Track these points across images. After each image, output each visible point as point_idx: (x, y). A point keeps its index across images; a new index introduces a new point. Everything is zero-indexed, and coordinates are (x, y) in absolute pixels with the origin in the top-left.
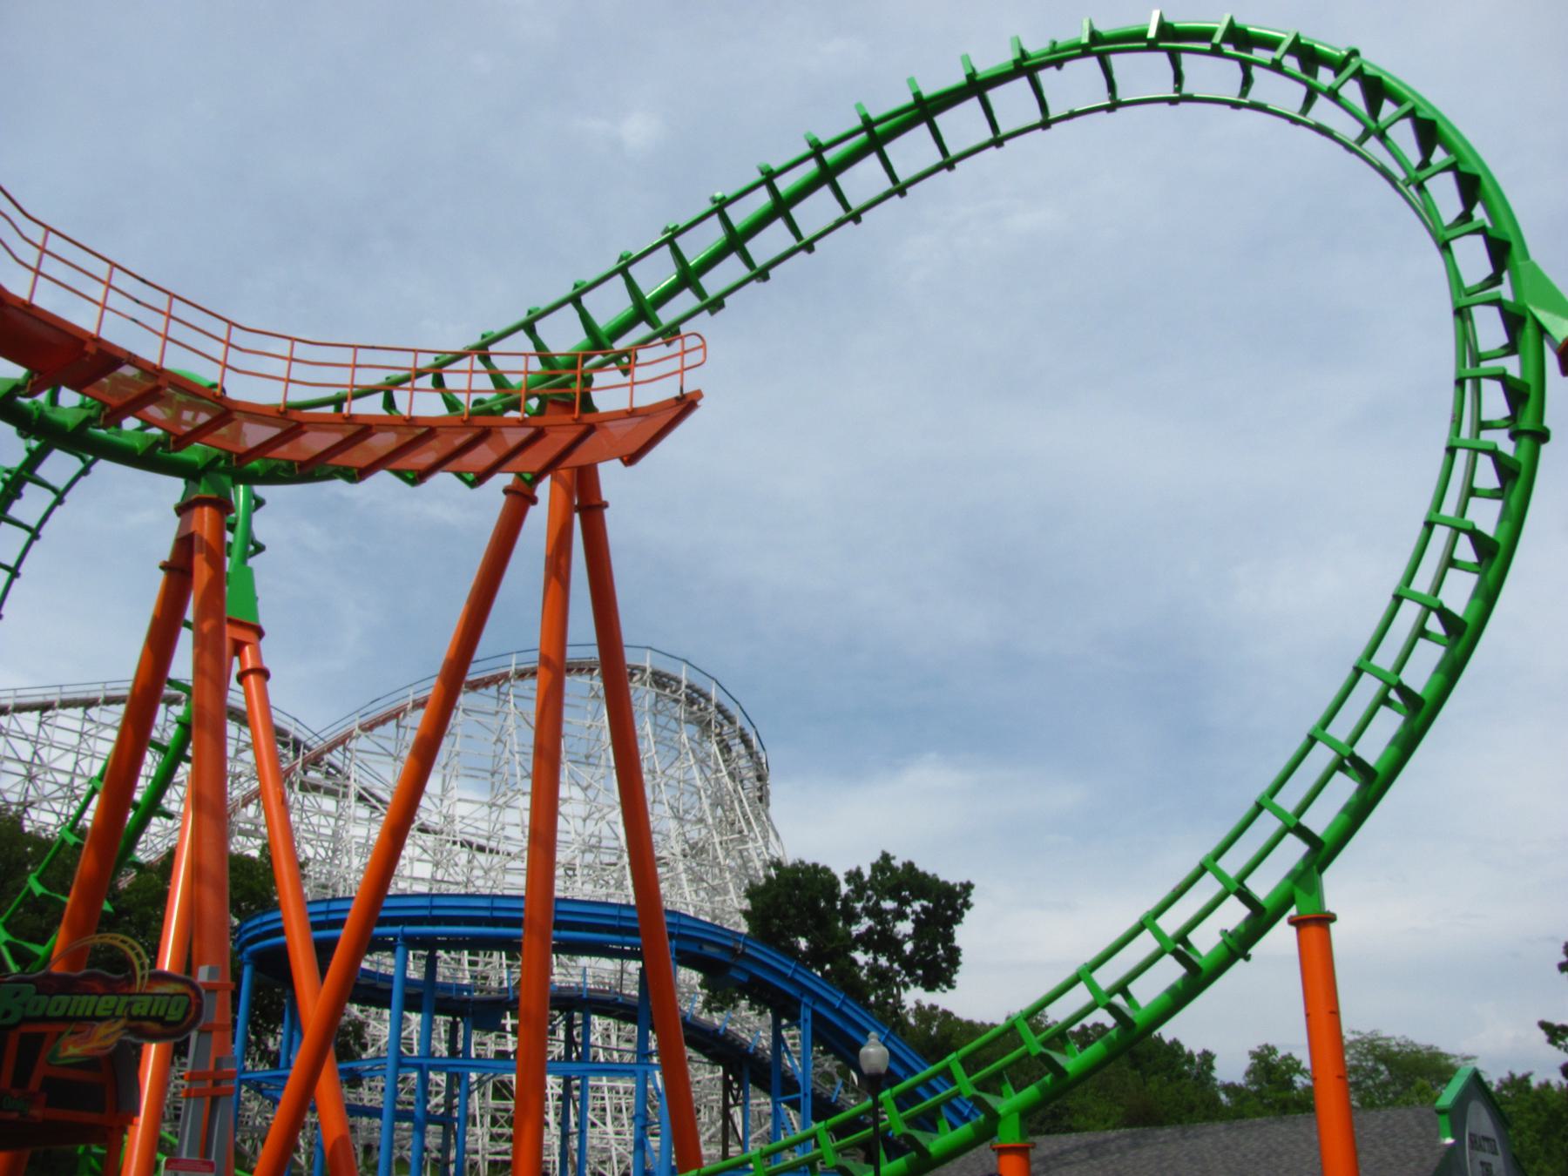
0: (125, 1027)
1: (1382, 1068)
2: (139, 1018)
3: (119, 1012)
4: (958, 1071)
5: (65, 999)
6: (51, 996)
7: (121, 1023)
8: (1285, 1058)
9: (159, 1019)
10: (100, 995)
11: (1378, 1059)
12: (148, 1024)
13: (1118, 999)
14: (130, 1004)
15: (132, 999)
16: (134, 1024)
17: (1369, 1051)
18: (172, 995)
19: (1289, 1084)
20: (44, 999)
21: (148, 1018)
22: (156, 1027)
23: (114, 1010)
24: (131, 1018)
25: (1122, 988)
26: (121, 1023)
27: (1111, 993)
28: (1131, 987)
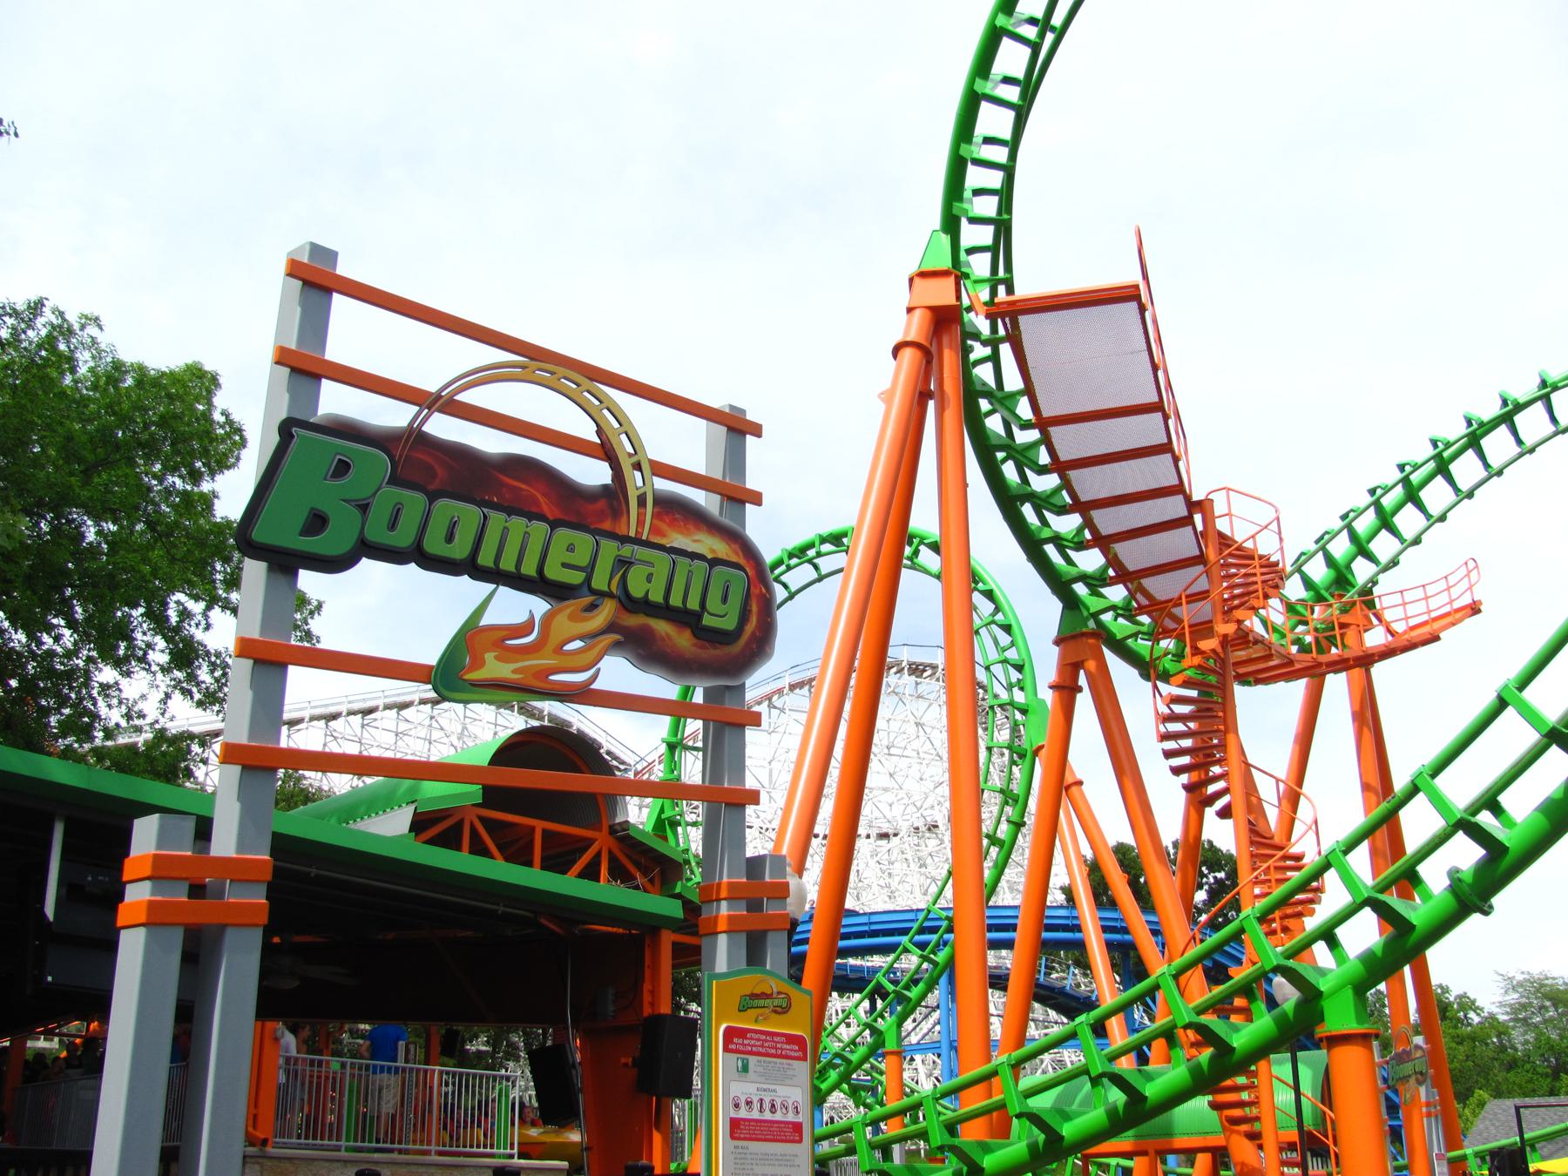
0: (611, 628)
1: (1548, 1003)
2: (644, 606)
3: (600, 582)
4: (1256, 932)
5: (469, 514)
6: (433, 497)
7: (607, 611)
8: (1460, 997)
9: (687, 619)
10: (554, 525)
11: (1546, 996)
12: (661, 627)
13: (1485, 818)
14: (623, 564)
15: (627, 550)
16: (634, 621)
17: (1538, 990)
18: (715, 562)
19: (1466, 1021)
20: (414, 501)
21: (664, 611)
22: (683, 640)
23: (590, 570)
24: (629, 603)
25: (1491, 802)
26: (607, 611)
27: (1475, 809)
28: (1503, 799)
